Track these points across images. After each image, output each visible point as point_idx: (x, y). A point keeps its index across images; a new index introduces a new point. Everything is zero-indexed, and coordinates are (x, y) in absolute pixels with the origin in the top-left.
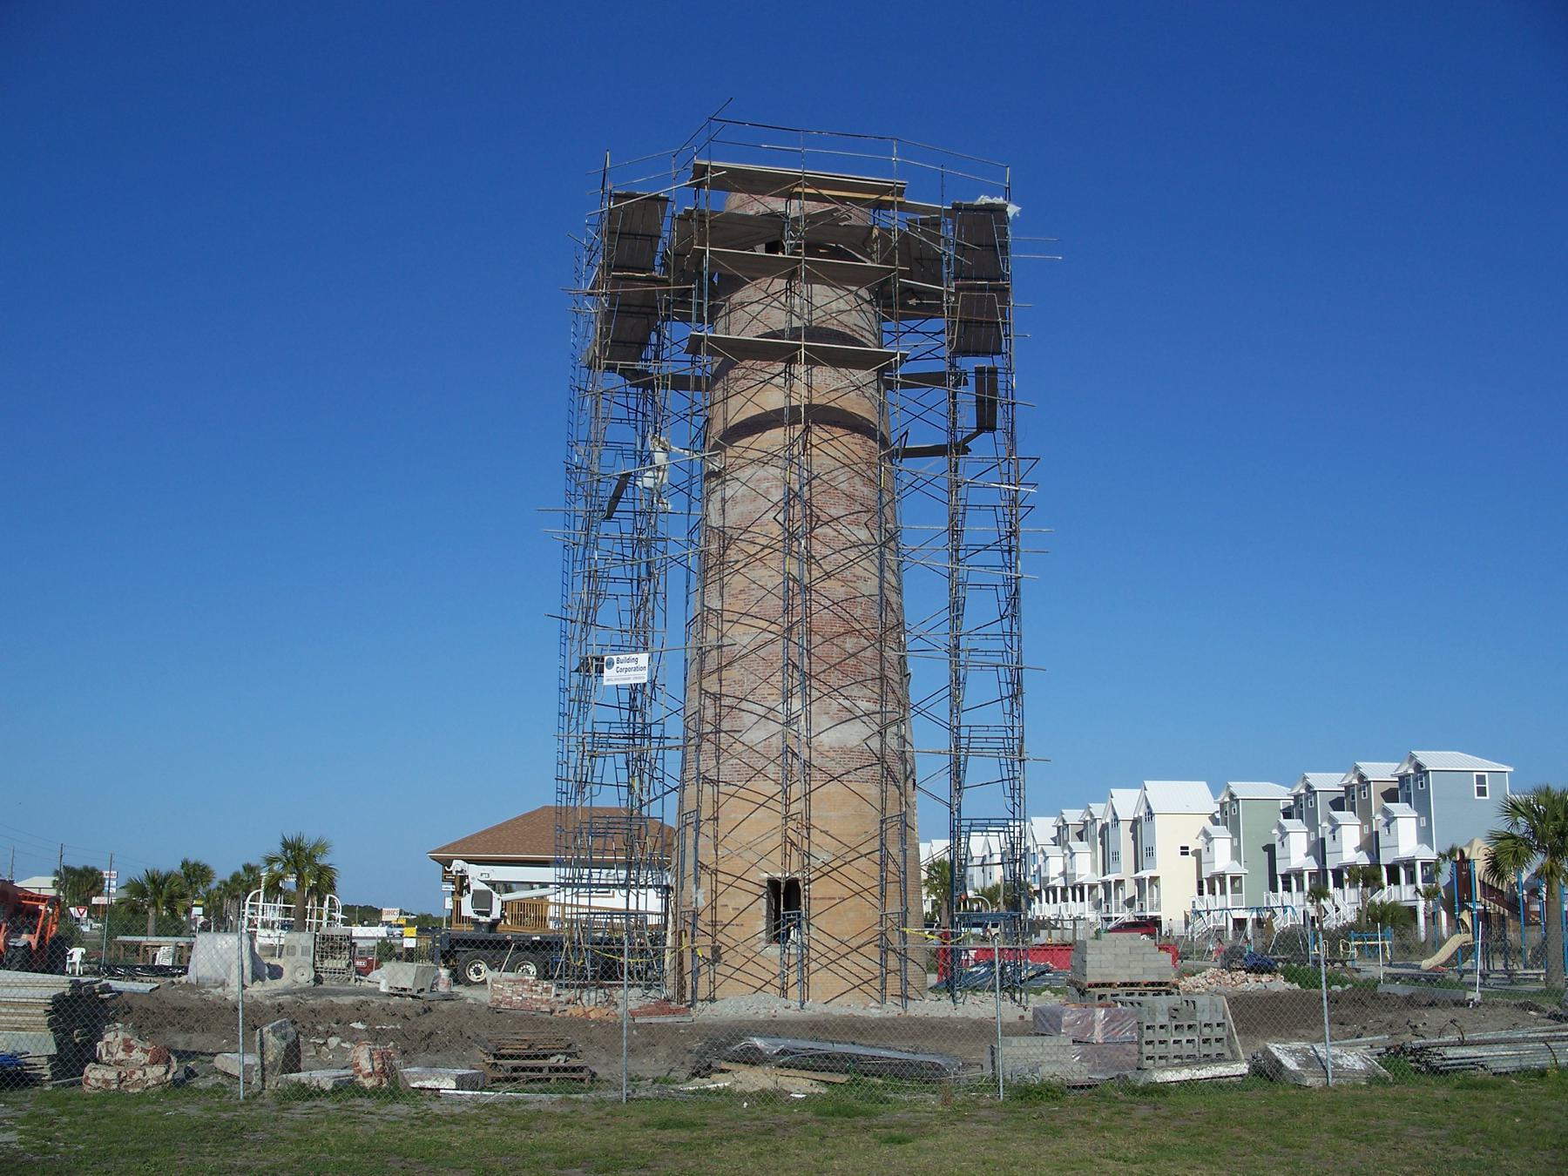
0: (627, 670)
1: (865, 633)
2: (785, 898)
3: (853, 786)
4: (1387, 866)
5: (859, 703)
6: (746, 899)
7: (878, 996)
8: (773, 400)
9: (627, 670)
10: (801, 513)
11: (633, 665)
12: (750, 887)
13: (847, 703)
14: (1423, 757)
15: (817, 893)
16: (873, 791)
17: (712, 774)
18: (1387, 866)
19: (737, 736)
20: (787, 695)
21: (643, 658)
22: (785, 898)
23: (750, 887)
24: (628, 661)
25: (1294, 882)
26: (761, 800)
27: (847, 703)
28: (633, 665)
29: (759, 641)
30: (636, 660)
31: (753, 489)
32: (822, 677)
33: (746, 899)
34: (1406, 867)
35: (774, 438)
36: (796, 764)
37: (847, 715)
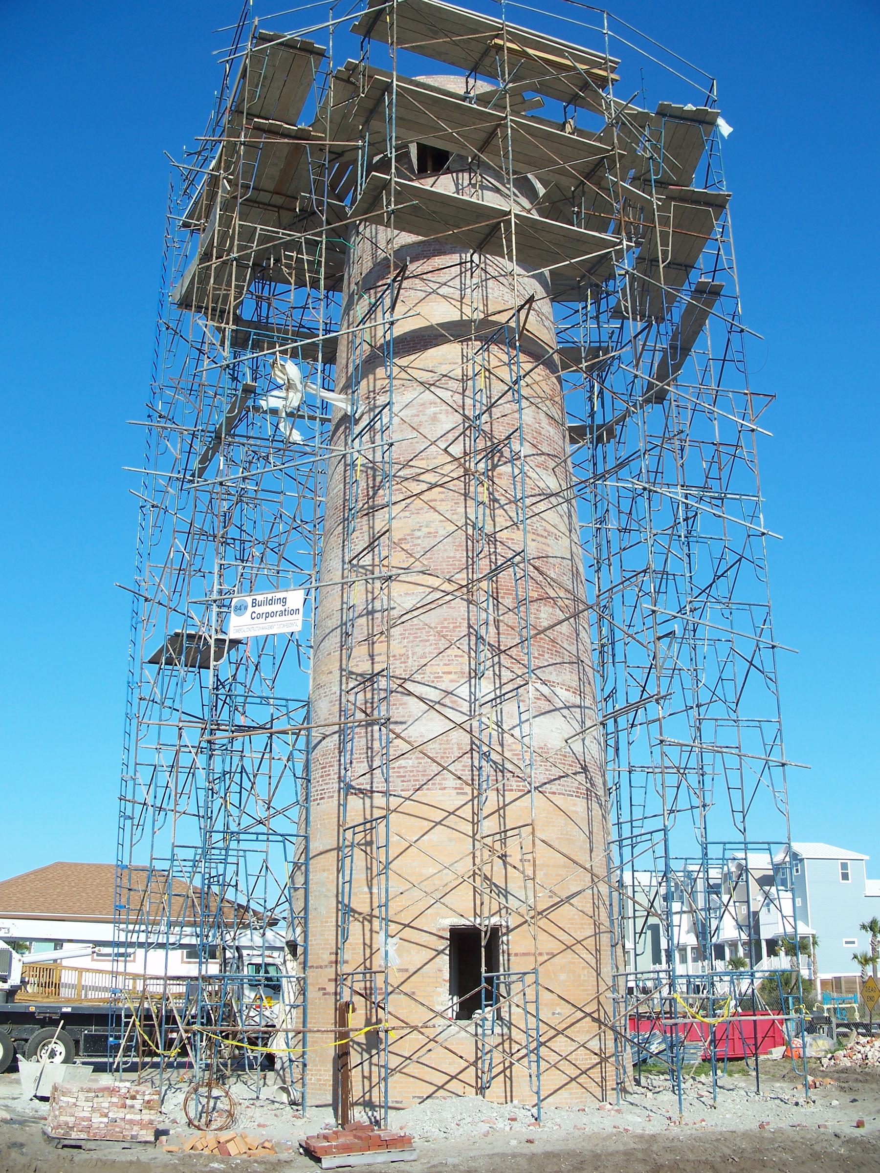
0: (268, 615)
1: (560, 603)
2: (472, 959)
3: (558, 800)
4: (767, 941)
5: (558, 690)
6: (420, 956)
7: (598, 1092)
8: (441, 312)
9: (268, 615)
10: (487, 450)
11: (278, 607)
12: (424, 938)
13: (545, 690)
14: (796, 847)
15: (518, 948)
16: (578, 807)
17: (364, 783)
18: (767, 941)
19: (398, 729)
20: (475, 675)
21: (295, 598)
22: (472, 959)
23: (424, 938)
24: (271, 602)
25: (677, 955)
26: (438, 816)
27: (545, 690)
28: (278, 607)
29: (429, 599)
30: (284, 601)
31: (421, 408)
32: (514, 652)
33: (420, 956)
34: (730, 945)
35: (446, 357)
36: (487, 764)
37: (545, 706)
